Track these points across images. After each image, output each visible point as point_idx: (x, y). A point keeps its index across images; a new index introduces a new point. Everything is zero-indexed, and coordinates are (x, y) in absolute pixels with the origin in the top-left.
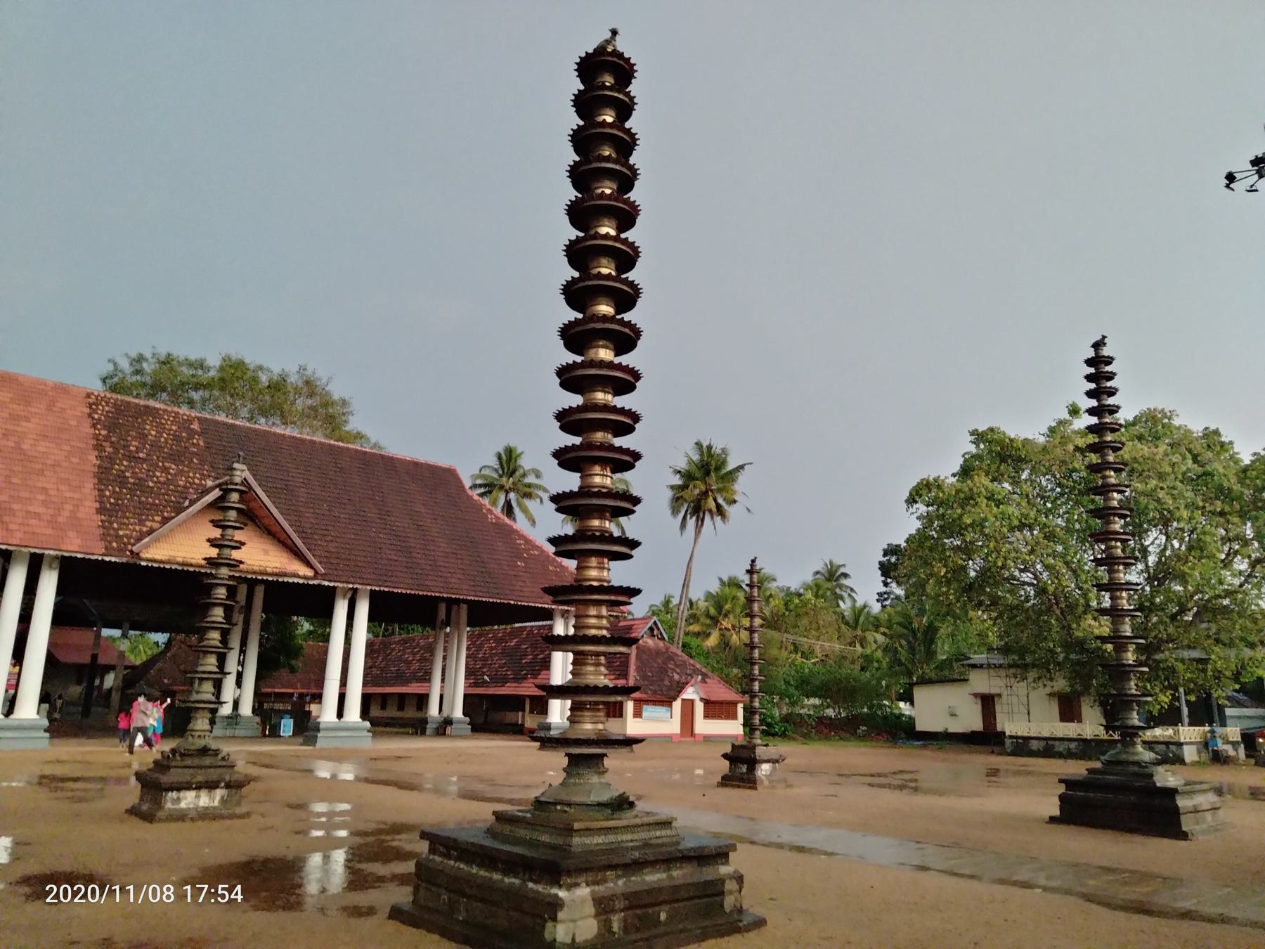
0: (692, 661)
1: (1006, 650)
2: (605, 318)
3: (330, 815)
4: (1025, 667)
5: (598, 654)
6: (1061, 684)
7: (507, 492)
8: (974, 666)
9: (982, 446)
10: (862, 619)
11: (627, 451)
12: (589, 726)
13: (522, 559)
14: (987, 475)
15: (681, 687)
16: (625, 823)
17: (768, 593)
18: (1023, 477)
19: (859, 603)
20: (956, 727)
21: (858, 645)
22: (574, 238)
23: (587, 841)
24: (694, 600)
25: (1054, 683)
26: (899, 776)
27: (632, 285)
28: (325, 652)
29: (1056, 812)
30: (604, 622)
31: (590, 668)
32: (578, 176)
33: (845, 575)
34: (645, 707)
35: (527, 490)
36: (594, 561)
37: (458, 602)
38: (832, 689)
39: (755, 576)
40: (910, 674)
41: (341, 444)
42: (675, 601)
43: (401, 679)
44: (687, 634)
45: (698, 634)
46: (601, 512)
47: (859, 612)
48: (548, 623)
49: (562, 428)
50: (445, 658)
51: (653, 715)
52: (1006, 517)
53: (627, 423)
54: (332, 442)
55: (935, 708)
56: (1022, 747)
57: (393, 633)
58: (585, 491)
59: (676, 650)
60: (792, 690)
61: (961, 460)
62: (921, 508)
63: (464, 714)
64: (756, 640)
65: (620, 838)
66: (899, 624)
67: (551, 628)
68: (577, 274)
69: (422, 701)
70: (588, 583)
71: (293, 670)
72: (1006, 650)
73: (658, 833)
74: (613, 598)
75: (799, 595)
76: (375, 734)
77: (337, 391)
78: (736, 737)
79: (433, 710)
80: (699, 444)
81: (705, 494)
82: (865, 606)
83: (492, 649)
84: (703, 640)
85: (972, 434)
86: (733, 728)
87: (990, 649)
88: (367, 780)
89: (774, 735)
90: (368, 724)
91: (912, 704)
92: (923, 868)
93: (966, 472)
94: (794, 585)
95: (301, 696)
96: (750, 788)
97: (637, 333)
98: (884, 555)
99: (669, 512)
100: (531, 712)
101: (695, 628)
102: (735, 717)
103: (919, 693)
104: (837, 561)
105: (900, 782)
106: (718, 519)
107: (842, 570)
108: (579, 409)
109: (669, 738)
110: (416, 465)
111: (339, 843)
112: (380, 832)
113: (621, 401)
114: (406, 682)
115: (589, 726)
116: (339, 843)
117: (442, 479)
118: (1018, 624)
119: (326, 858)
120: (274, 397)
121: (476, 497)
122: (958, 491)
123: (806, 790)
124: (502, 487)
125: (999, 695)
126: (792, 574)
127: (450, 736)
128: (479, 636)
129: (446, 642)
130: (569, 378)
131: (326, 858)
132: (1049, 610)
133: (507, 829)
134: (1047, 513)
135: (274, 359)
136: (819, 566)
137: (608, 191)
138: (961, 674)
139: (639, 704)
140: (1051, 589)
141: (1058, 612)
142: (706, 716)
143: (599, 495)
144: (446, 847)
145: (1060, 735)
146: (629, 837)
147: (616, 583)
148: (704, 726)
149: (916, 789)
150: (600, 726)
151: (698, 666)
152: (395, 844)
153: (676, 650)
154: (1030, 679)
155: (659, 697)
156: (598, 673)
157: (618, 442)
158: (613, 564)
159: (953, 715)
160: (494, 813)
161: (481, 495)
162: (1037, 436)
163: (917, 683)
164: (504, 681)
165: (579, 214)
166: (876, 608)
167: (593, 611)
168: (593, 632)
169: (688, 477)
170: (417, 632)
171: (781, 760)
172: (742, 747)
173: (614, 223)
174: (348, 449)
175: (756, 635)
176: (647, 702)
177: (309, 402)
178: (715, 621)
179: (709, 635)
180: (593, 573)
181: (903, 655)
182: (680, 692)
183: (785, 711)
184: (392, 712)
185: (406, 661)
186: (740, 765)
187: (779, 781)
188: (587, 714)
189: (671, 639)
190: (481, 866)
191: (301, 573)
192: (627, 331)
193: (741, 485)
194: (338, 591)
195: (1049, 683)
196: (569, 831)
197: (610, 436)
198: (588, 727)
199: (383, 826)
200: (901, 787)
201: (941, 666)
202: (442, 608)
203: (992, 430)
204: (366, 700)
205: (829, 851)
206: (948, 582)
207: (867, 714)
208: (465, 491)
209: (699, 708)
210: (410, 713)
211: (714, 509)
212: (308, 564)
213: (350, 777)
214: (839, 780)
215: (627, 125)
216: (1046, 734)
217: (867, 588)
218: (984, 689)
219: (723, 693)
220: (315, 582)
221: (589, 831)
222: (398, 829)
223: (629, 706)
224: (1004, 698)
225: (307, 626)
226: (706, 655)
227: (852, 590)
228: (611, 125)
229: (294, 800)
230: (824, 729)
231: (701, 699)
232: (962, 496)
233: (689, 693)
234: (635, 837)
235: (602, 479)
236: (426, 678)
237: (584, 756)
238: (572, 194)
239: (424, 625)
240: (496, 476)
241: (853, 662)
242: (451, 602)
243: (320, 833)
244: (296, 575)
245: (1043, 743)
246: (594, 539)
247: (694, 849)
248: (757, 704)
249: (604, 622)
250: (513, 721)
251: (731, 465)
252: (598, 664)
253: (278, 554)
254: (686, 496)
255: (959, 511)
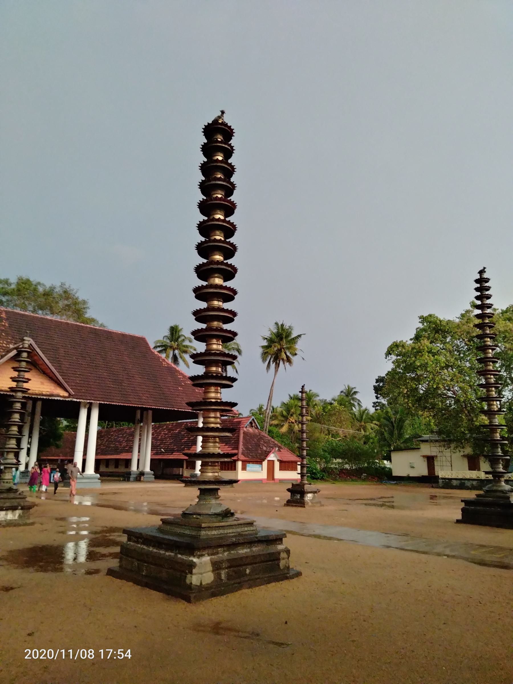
0: (273, 440)
1: (440, 433)
2: (218, 263)
3: (78, 523)
4: (450, 441)
5: (215, 437)
6: (469, 450)
7: (174, 350)
8: (423, 441)
9: (425, 324)
10: (364, 417)
11: (230, 332)
12: (210, 474)
13: (181, 386)
14: (428, 339)
15: (267, 454)
16: (229, 523)
17: (314, 403)
18: (448, 340)
19: (363, 408)
20: (413, 473)
21: (362, 430)
22: (202, 220)
23: (209, 533)
24: (275, 407)
25: (465, 450)
26: (381, 500)
27: (232, 245)
28: (75, 437)
29: (460, 517)
30: (218, 420)
31: (211, 444)
32: (205, 188)
33: (355, 393)
34: (248, 464)
35: (185, 349)
36: (213, 389)
37: (147, 409)
38: (349, 454)
39: (304, 395)
40: (389, 446)
41: (83, 325)
42: (265, 408)
43: (117, 451)
44: (271, 425)
45: (276, 426)
46: (216, 363)
47: (363, 412)
48: (197, 420)
49: (196, 319)
50: (140, 440)
51: (253, 469)
52: (437, 362)
53: (230, 317)
54: (78, 324)
55: (402, 464)
56: (448, 484)
57: (112, 427)
58: (208, 352)
59: (265, 434)
60: (327, 454)
61: (415, 332)
62: (394, 357)
63: (151, 469)
64: (305, 428)
65: (226, 531)
66: (384, 418)
67: (197, 423)
68: (203, 239)
69: (128, 463)
70: (210, 400)
71: (57, 447)
72: (439, 433)
73: (246, 529)
74: (223, 408)
75: (331, 404)
76: (102, 481)
77: (81, 296)
78: (296, 480)
79: (134, 468)
80: (277, 324)
81: (280, 350)
82: (366, 410)
83: (165, 434)
84: (280, 429)
85: (420, 318)
86: (294, 475)
87: (432, 432)
88: (98, 505)
89: (317, 479)
90: (98, 475)
91: (391, 461)
92: (388, 547)
93: (417, 338)
94: (329, 399)
95: (62, 460)
96: (301, 507)
97: (235, 270)
98: (376, 382)
99: (261, 360)
100: (187, 468)
101: (275, 422)
102: (296, 469)
103: (394, 456)
104: (352, 386)
105: (381, 503)
106: (287, 364)
107: (354, 390)
108: (205, 310)
109: (261, 481)
110: (124, 335)
111: (83, 537)
112: (102, 532)
113: (226, 306)
114: (118, 453)
115: (210, 474)
116: (83, 537)
117: (138, 343)
118: (445, 418)
119: (77, 545)
120: (47, 299)
121: (156, 353)
122: (413, 348)
123: (330, 508)
124: (171, 347)
125: (437, 456)
126: (327, 392)
127: (143, 481)
128: (159, 427)
129: (141, 431)
130: (200, 294)
131: (77, 545)
132: (462, 411)
133: (168, 527)
134: (461, 359)
135: (46, 279)
136: (343, 388)
137: (220, 196)
138: (417, 445)
139: (245, 463)
140: (462, 400)
141: (466, 412)
142: (281, 469)
143: (215, 354)
144: (136, 537)
145: (468, 477)
146: (231, 531)
147: (224, 400)
148: (279, 474)
149: (393, 507)
150: (216, 474)
151: (276, 442)
152: (111, 538)
153: (265, 434)
154: (452, 448)
155: (255, 460)
156: (215, 447)
157: (226, 327)
158: (223, 390)
159: (413, 467)
160: (162, 520)
161: (160, 352)
162: (455, 319)
163: (395, 450)
164: (172, 451)
165: (205, 208)
166: (372, 410)
167: (212, 415)
168: (213, 425)
169: (271, 341)
170: (125, 426)
171: (322, 493)
172: (297, 485)
173: (223, 213)
174: (87, 327)
175: (305, 426)
176: (249, 462)
177: (66, 302)
178: (286, 418)
179: (282, 426)
180: (213, 395)
181: (386, 435)
182: (266, 456)
183: (323, 466)
184: (112, 469)
185: (119, 441)
186: (297, 494)
187: (317, 503)
188: (210, 468)
189: (262, 428)
190: (154, 546)
191: (61, 395)
192: (230, 269)
193: (299, 345)
194: (82, 405)
195: (462, 450)
196: (199, 528)
197: (221, 324)
198: (210, 475)
199: (105, 529)
200: (382, 506)
201: (406, 441)
202: (139, 412)
203: (430, 316)
204: (98, 463)
205: (340, 538)
206: (408, 397)
207: (367, 467)
208: (150, 349)
209: (277, 465)
210: (122, 469)
211: (285, 358)
212: (66, 390)
213: (89, 503)
214: (349, 502)
215: (230, 161)
216: (460, 477)
217: (367, 400)
218: (429, 454)
219: (291, 457)
220: (69, 399)
221: (210, 528)
222: (112, 530)
223: (239, 464)
224: (439, 458)
225: (65, 423)
226: (282, 436)
227: (359, 401)
228: (221, 162)
229: (58, 516)
230: (344, 475)
231: (278, 460)
232: (415, 351)
233: (272, 457)
234: (234, 530)
235: (217, 346)
236: (130, 450)
237: (208, 490)
238: (201, 197)
239: (129, 422)
240: (168, 341)
241: (359, 440)
242: (143, 410)
243: (73, 533)
244: (58, 396)
245: (458, 482)
246: (213, 377)
247: (265, 537)
248: (305, 462)
249: (218, 420)
250: (177, 473)
251: (293, 336)
252: (215, 442)
253: (49, 384)
254: (269, 352)
255: (414, 359)
